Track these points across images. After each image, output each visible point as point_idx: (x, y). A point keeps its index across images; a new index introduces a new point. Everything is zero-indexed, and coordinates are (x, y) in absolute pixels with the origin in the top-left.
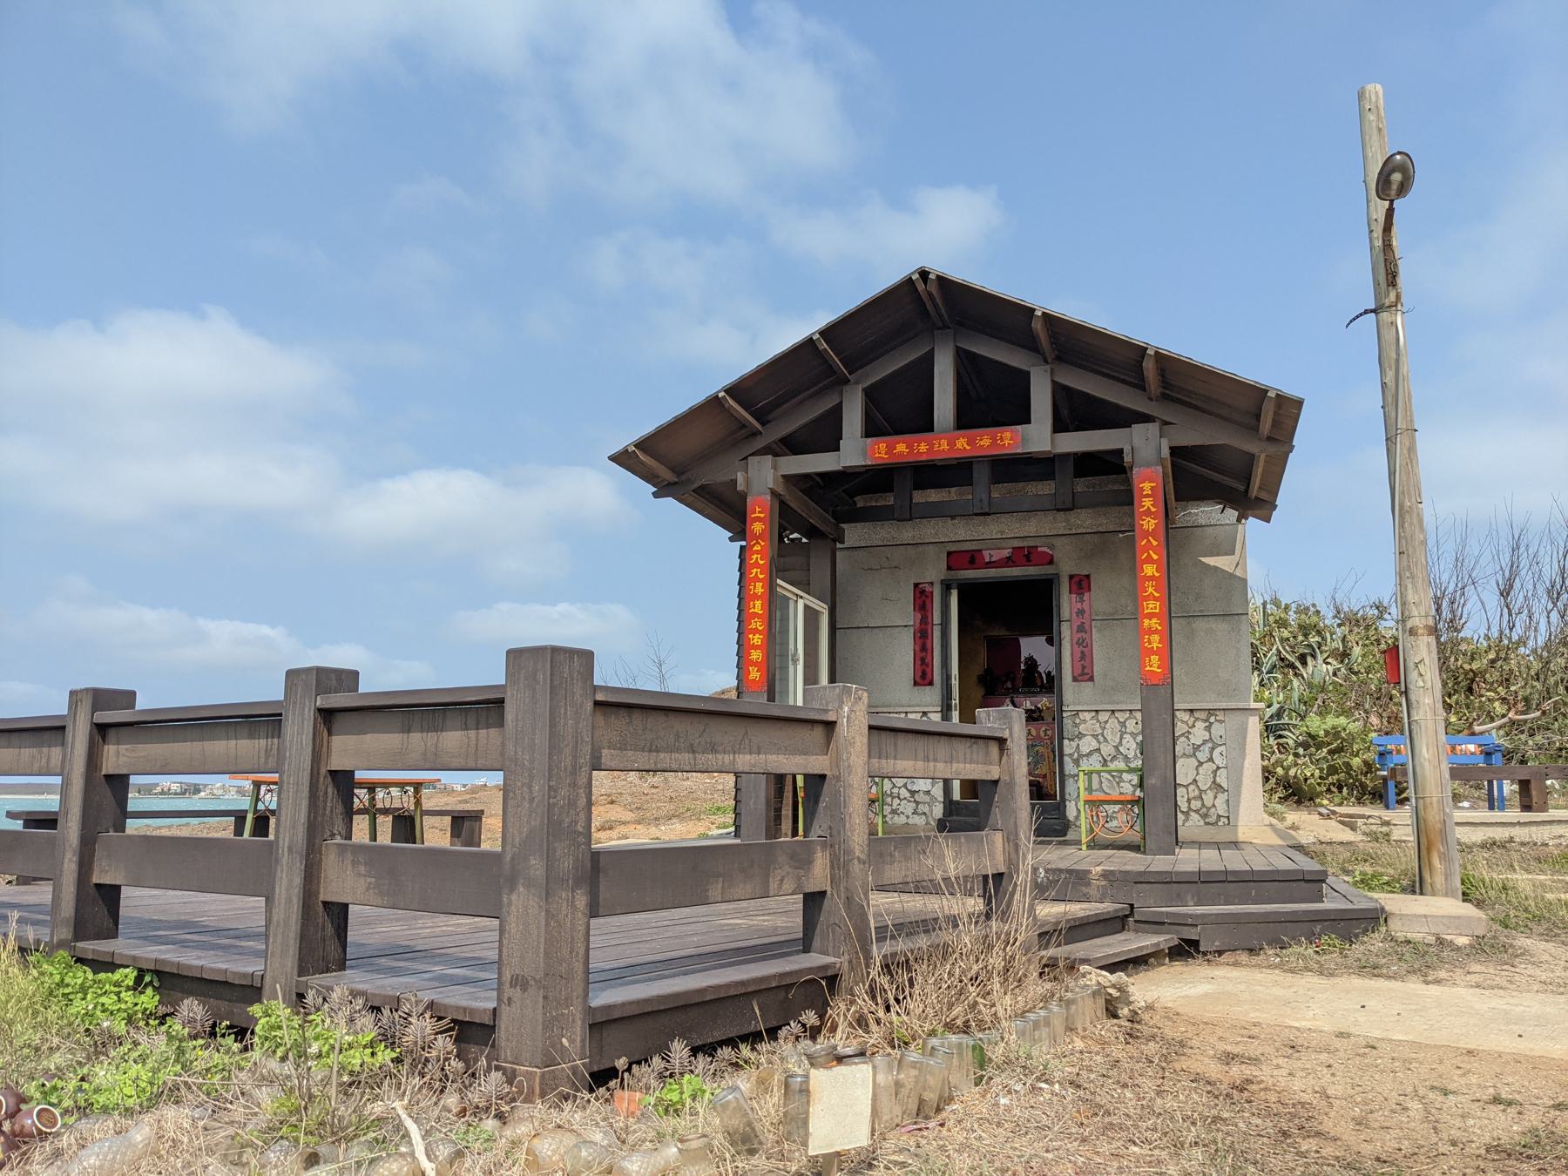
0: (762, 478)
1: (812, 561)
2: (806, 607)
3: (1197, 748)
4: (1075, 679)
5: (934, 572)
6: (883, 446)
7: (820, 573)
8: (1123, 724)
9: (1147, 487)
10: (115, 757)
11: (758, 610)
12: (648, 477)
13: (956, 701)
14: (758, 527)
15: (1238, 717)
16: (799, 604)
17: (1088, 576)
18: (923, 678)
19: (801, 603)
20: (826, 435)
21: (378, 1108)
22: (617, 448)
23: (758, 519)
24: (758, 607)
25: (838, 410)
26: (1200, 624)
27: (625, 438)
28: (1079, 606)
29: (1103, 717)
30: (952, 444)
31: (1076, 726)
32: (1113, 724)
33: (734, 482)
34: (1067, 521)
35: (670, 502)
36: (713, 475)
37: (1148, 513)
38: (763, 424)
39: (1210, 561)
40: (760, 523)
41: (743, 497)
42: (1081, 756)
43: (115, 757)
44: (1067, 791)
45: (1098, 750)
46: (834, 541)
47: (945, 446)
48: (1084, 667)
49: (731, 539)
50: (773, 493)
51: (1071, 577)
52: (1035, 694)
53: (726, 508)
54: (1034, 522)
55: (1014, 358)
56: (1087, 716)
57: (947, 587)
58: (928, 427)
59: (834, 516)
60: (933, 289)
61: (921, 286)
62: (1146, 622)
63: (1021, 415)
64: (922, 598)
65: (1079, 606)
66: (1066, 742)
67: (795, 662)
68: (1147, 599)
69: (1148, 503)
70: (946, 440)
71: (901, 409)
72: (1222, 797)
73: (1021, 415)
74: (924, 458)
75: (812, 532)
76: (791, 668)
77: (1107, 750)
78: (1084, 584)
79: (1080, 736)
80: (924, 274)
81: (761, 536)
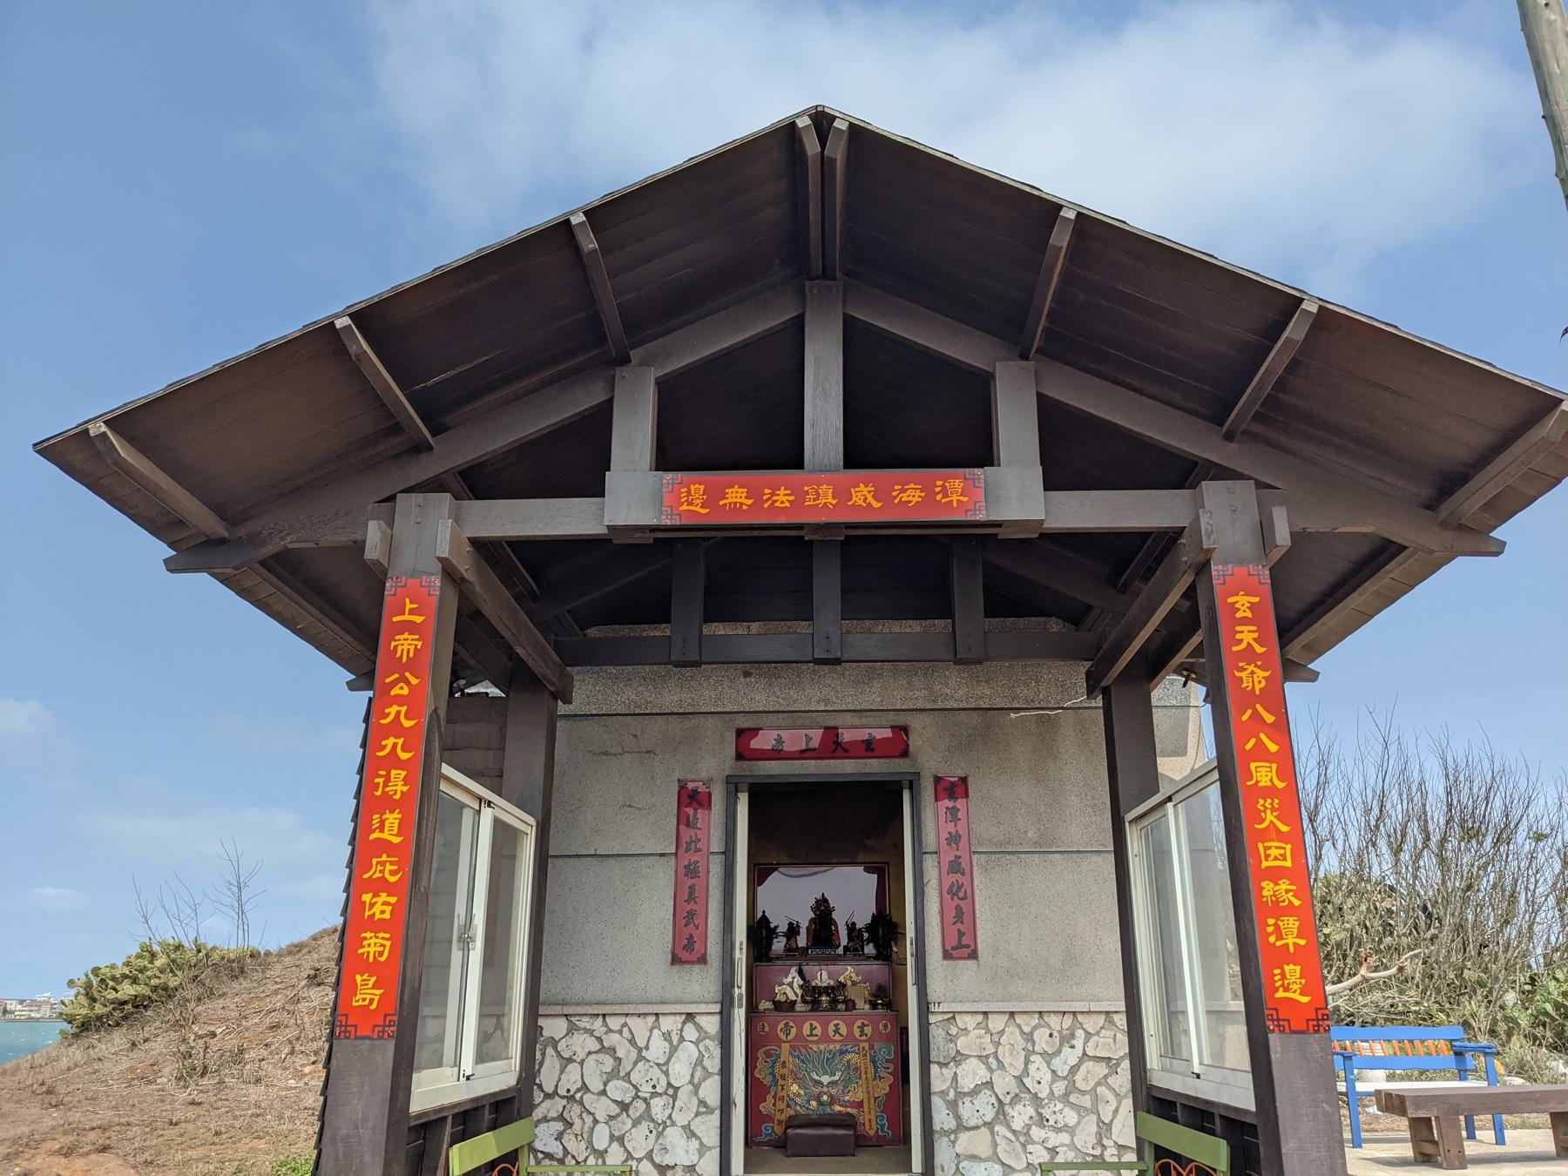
0: (424, 542)
1: (510, 732)
2: (498, 825)
4: (947, 955)
5: (713, 764)
6: (698, 490)
7: (524, 757)
8: (1029, 1037)
9: (1243, 603)
11: (391, 835)
12: (160, 523)
13: (740, 991)
14: (405, 645)
16: (484, 819)
17: (964, 780)
18: (685, 952)
19: (487, 816)
20: (577, 463)
21: (71, 1138)
22: (62, 422)
23: (409, 627)
24: (390, 828)
27: (89, 403)
28: (951, 827)
29: (996, 1023)
30: (842, 495)
31: (952, 1039)
32: (1012, 1037)
33: (359, 546)
34: (929, 688)
35: (203, 586)
36: (303, 530)
37: (1249, 655)
38: (434, 433)
40: (413, 632)
41: (376, 577)
42: (960, 1095)
44: (938, 1161)
45: (989, 1084)
46: (555, 696)
47: (827, 497)
48: (961, 934)
49: (352, 686)
50: (449, 572)
51: (938, 780)
52: (836, 959)
53: (335, 607)
54: (876, 685)
55: (963, 348)
56: (969, 1022)
57: (733, 785)
58: (795, 460)
59: (558, 648)
60: (838, 151)
61: (812, 146)
62: (1268, 888)
63: (982, 453)
64: (691, 799)
65: (951, 827)
66: (934, 1069)
67: (466, 942)
68: (1264, 836)
69: (1247, 635)
70: (825, 489)
71: (734, 421)
73: (982, 453)
74: (782, 520)
75: (517, 678)
76: (456, 956)
77: (1004, 1083)
78: (960, 790)
79: (959, 1058)
80: (822, 120)
81: (412, 665)
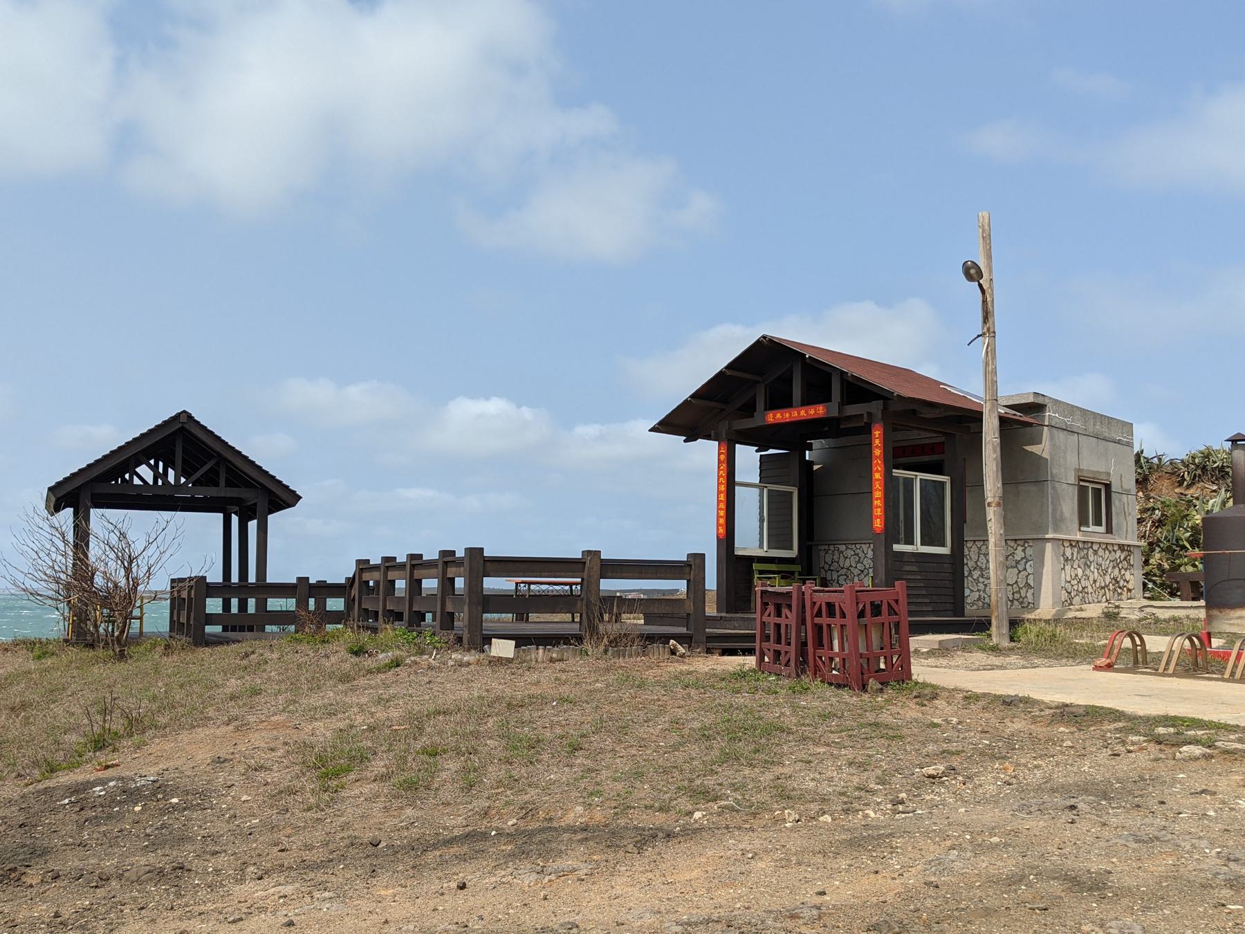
3: (1017, 562)
8: (980, 549)
10: (417, 574)
15: (1039, 543)
25: (754, 398)
26: (1023, 488)
39: (1029, 448)
43: (417, 574)
72: (1031, 591)
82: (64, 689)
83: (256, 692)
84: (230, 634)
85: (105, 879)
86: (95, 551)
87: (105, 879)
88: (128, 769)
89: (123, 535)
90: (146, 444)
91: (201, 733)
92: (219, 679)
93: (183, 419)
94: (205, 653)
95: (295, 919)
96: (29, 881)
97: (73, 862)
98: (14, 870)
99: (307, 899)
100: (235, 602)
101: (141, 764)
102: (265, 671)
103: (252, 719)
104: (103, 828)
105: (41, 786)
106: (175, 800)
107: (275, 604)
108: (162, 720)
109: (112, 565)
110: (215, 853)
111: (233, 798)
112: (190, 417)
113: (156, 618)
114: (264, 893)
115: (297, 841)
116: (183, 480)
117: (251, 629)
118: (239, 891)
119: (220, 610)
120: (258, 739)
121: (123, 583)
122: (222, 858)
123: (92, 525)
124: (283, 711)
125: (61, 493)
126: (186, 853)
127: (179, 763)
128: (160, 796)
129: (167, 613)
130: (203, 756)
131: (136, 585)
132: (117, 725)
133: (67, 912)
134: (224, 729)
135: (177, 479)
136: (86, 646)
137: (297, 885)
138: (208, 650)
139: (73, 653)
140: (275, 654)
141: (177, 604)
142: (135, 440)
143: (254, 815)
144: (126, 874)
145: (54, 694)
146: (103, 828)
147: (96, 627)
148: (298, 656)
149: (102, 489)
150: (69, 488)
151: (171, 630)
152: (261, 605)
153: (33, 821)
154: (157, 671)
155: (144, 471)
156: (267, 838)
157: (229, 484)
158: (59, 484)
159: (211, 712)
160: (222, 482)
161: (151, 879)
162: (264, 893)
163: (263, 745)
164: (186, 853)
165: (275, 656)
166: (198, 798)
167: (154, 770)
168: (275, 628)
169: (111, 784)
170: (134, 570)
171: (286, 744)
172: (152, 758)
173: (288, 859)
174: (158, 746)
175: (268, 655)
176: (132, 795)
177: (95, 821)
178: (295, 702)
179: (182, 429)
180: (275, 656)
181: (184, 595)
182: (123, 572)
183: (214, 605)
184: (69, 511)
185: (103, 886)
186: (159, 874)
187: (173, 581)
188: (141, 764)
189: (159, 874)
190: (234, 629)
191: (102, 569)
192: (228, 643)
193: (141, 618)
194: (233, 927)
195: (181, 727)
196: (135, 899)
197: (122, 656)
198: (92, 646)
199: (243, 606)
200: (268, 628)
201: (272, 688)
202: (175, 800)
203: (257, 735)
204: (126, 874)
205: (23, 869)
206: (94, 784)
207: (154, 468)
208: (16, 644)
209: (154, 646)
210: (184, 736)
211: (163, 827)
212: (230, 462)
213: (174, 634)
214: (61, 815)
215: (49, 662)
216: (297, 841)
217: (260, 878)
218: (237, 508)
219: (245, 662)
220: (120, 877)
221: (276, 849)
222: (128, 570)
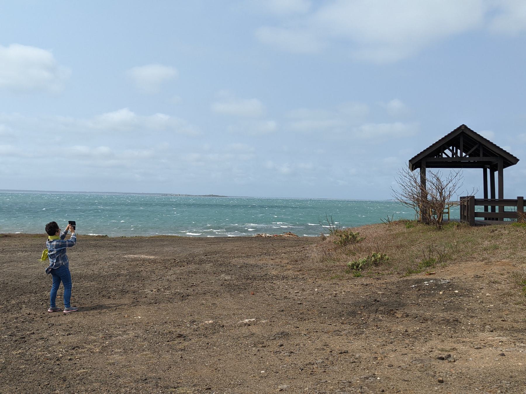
82: (417, 241)
83: (496, 248)
84: (488, 221)
85: (426, 320)
86: (428, 185)
87: (426, 320)
88: (439, 276)
89: (438, 179)
90: (447, 140)
91: (470, 264)
92: (480, 240)
93: (463, 128)
94: (475, 229)
95: (505, 353)
96: (397, 316)
97: (414, 311)
98: (392, 310)
99: (513, 345)
100: (489, 207)
101: (445, 274)
102: (501, 239)
103: (493, 260)
104: (427, 299)
105: (405, 279)
106: (457, 291)
107: (508, 209)
108: (454, 257)
109: (434, 191)
110: (472, 317)
111: (483, 294)
112: (466, 127)
113: (454, 213)
114: (493, 339)
115: (510, 318)
116: (464, 154)
117: (497, 219)
118: (482, 335)
119: (483, 211)
120: (495, 269)
121: (438, 198)
122: (475, 320)
123: (426, 177)
124: (508, 257)
125: (414, 162)
126: (460, 315)
127: (460, 276)
128: (450, 289)
129: (459, 211)
130: (471, 274)
131: (444, 201)
132: (436, 257)
133: (410, 331)
134: (480, 263)
135: (461, 154)
136: (426, 223)
137: (508, 338)
138: (476, 228)
139: (420, 226)
140: (507, 231)
141: (463, 208)
142: (443, 139)
143: (491, 303)
144: (434, 319)
145: (412, 242)
146: (427, 299)
147: (430, 216)
148: (517, 233)
149: (430, 160)
150: (417, 160)
151: (461, 218)
152: (502, 209)
153: (401, 292)
154: (454, 236)
155: (447, 151)
156: (497, 314)
157: (484, 155)
158: (413, 159)
159: (475, 255)
160: (481, 154)
161: (444, 323)
162: (493, 339)
163: (497, 272)
164: (460, 315)
165: (507, 232)
166: (467, 292)
167: (449, 277)
168: (509, 220)
169: (431, 281)
170: (443, 193)
171: (508, 273)
172: (449, 272)
173: (506, 325)
174: (451, 268)
175: (503, 231)
176: (440, 287)
177: (424, 295)
178: (514, 254)
179: (463, 132)
180: (507, 232)
181: (466, 204)
182: (438, 194)
183: (479, 209)
184: (418, 169)
185: (425, 323)
186: (447, 322)
187: (461, 198)
188: (445, 274)
189: (447, 322)
190: (489, 219)
191: (430, 193)
192: (485, 225)
193: (448, 213)
194: (476, 351)
195: (462, 260)
196: (437, 330)
197: (440, 229)
198: (428, 224)
199: (493, 209)
200: (505, 219)
201: (504, 246)
202: (457, 291)
203: (495, 267)
204: (434, 319)
205: (395, 311)
206: (424, 280)
207: (452, 151)
208: (400, 221)
209: (453, 225)
210: (463, 265)
211: (451, 302)
212: (485, 146)
213: (462, 220)
214: (411, 291)
215: (411, 229)
216: (510, 318)
217: (492, 331)
218: (489, 166)
219: (492, 234)
220: (432, 320)
221: (500, 319)
222: (441, 193)
